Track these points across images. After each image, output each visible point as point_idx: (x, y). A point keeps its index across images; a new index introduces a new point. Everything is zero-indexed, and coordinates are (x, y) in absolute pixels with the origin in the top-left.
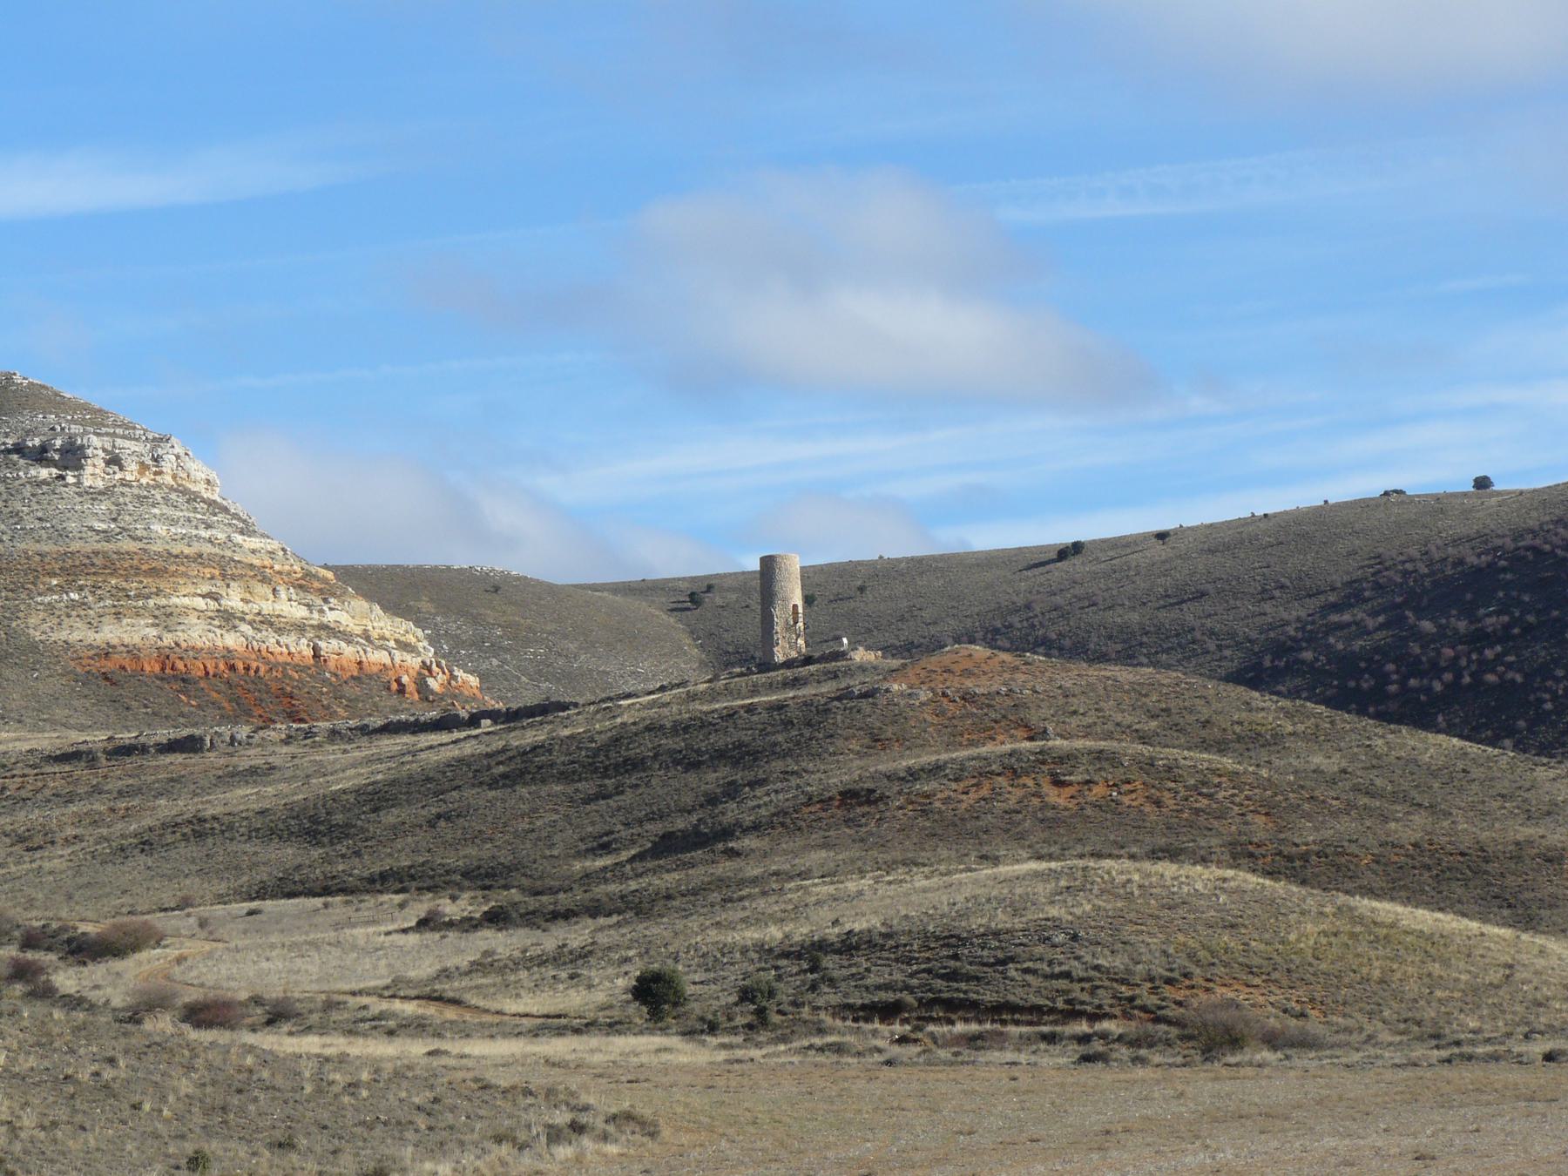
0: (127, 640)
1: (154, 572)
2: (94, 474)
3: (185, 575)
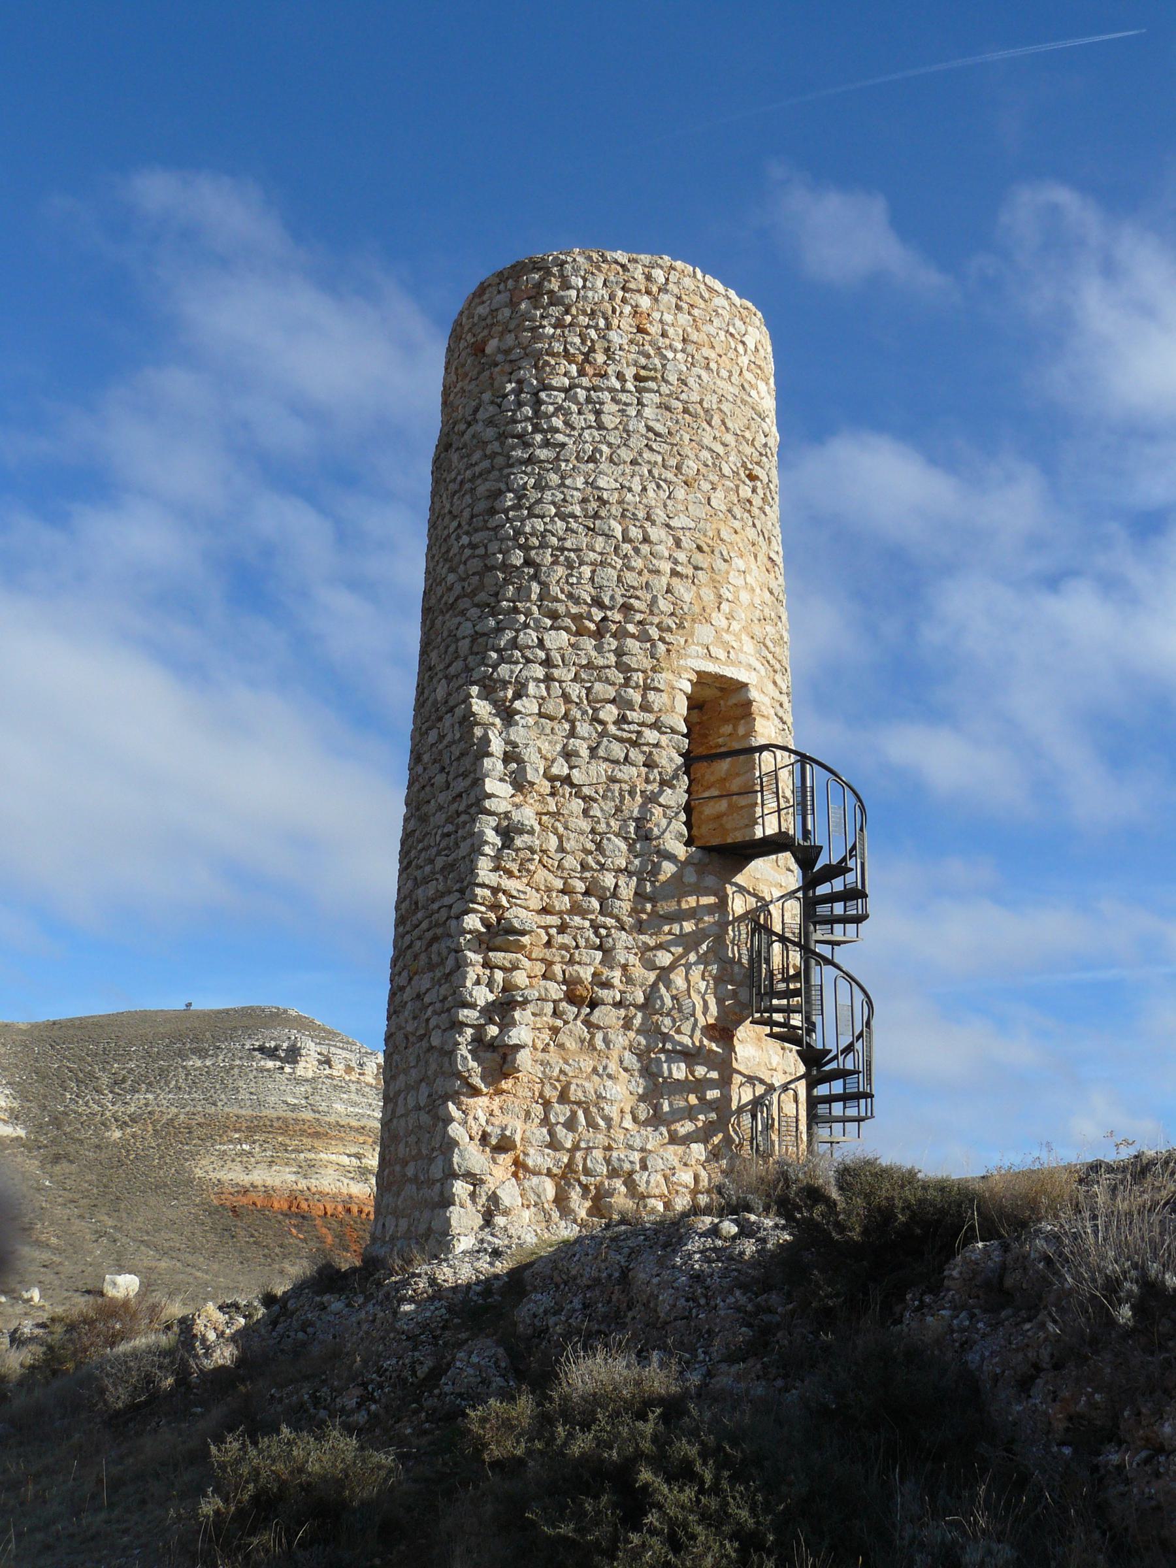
0: (269, 1182)
1: (317, 1135)
2: (307, 1067)
3: (342, 1139)
